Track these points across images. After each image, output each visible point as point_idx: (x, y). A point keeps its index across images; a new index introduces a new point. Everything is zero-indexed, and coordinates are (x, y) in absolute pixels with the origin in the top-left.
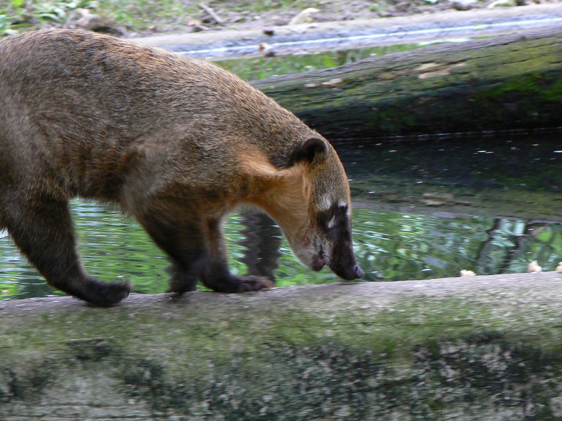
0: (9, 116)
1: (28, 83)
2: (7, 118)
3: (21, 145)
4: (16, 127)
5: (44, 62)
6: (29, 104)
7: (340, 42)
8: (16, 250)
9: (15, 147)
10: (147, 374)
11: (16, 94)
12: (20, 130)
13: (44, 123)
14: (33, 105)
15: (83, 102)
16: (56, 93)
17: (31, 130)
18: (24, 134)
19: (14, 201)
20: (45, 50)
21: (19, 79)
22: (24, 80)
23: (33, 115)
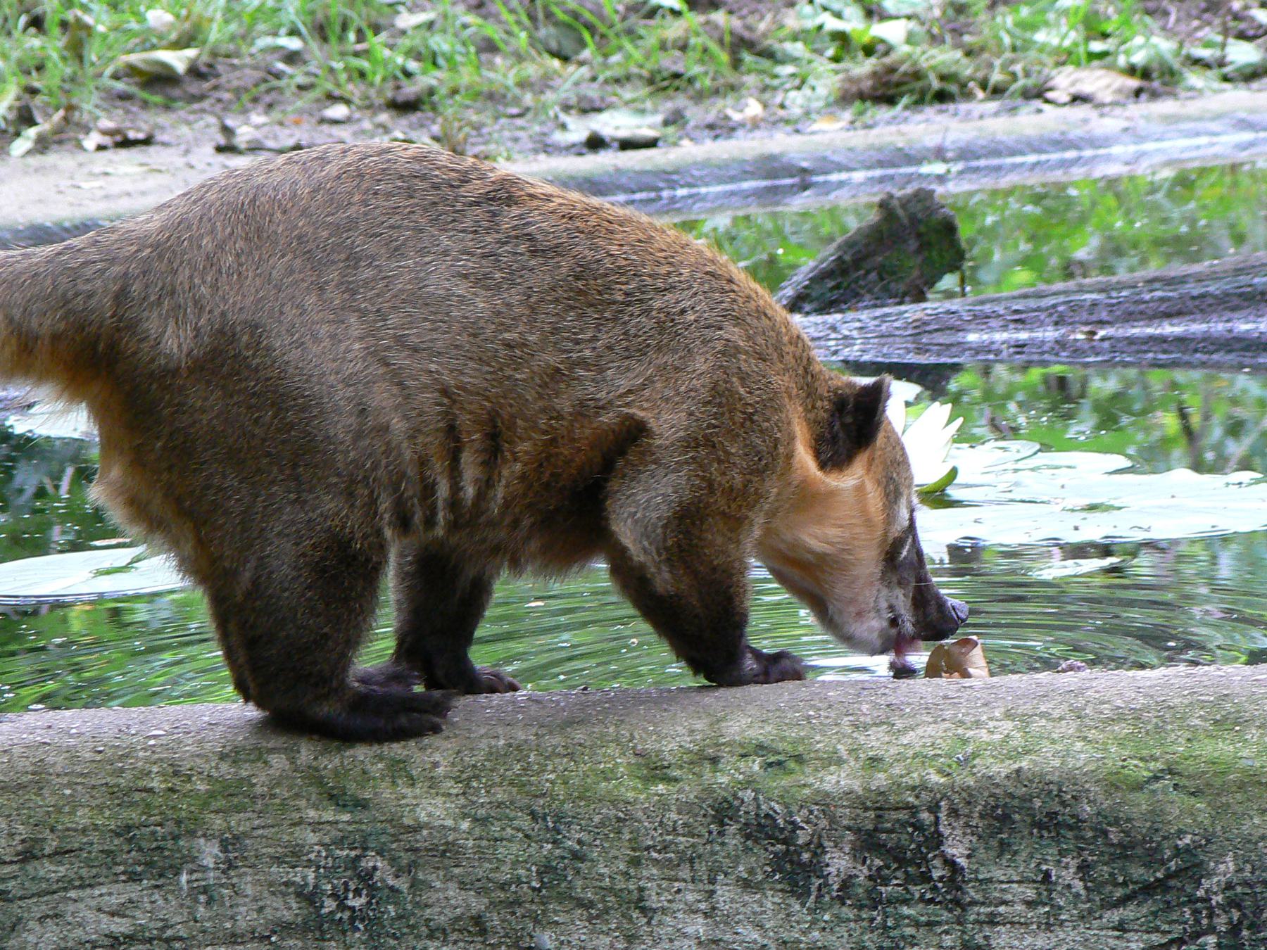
0: (316, 340)
1: (356, 267)
2: (309, 344)
3: (337, 410)
4: (329, 366)
5: (392, 221)
6: (363, 313)
7: (1213, 144)
8: (629, 604)
9: (321, 412)
10: (1236, 915)
11: (330, 288)
12: (337, 373)
13: (400, 359)
14: (372, 317)
15: (499, 313)
16: (431, 289)
17: (671, 232)
18: (347, 382)
19: (288, 535)
20: (389, 195)
21: (335, 257)
22: (347, 259)
23: (372, 340)
